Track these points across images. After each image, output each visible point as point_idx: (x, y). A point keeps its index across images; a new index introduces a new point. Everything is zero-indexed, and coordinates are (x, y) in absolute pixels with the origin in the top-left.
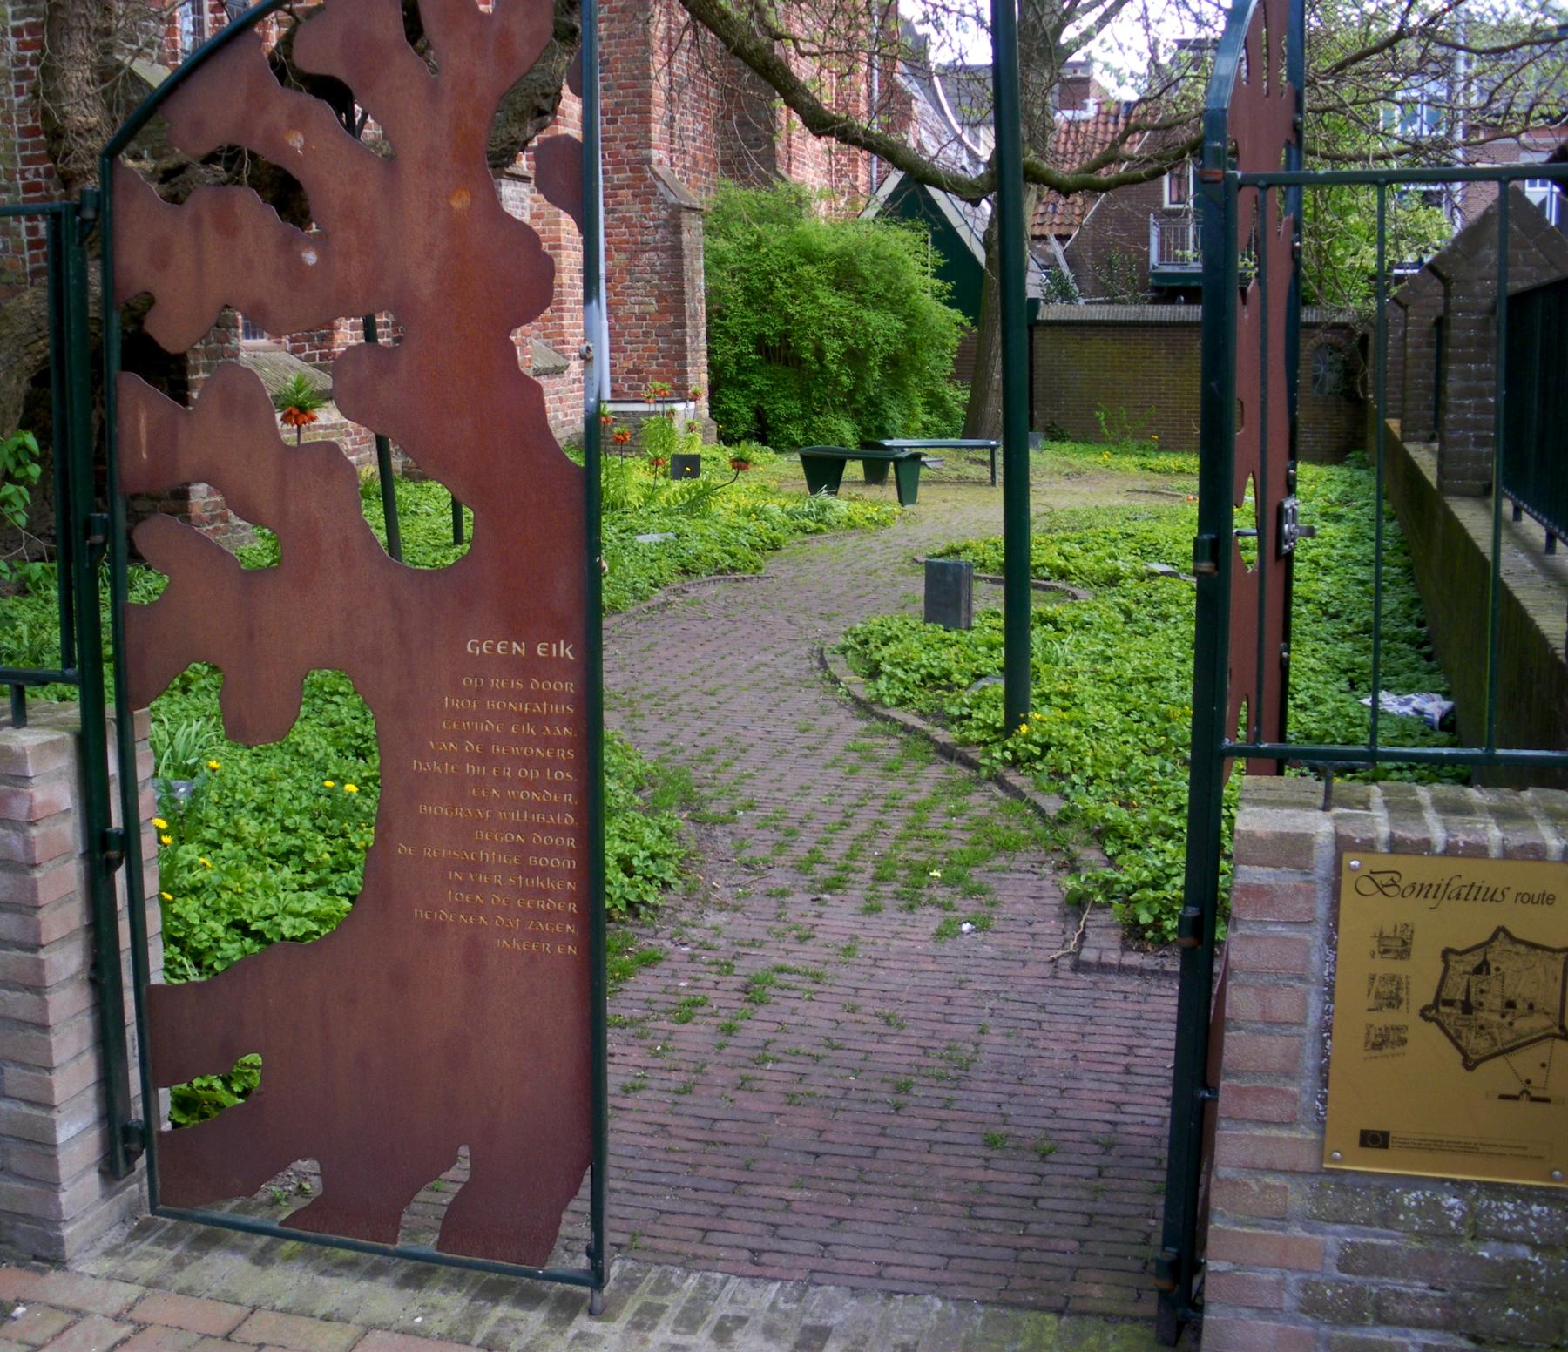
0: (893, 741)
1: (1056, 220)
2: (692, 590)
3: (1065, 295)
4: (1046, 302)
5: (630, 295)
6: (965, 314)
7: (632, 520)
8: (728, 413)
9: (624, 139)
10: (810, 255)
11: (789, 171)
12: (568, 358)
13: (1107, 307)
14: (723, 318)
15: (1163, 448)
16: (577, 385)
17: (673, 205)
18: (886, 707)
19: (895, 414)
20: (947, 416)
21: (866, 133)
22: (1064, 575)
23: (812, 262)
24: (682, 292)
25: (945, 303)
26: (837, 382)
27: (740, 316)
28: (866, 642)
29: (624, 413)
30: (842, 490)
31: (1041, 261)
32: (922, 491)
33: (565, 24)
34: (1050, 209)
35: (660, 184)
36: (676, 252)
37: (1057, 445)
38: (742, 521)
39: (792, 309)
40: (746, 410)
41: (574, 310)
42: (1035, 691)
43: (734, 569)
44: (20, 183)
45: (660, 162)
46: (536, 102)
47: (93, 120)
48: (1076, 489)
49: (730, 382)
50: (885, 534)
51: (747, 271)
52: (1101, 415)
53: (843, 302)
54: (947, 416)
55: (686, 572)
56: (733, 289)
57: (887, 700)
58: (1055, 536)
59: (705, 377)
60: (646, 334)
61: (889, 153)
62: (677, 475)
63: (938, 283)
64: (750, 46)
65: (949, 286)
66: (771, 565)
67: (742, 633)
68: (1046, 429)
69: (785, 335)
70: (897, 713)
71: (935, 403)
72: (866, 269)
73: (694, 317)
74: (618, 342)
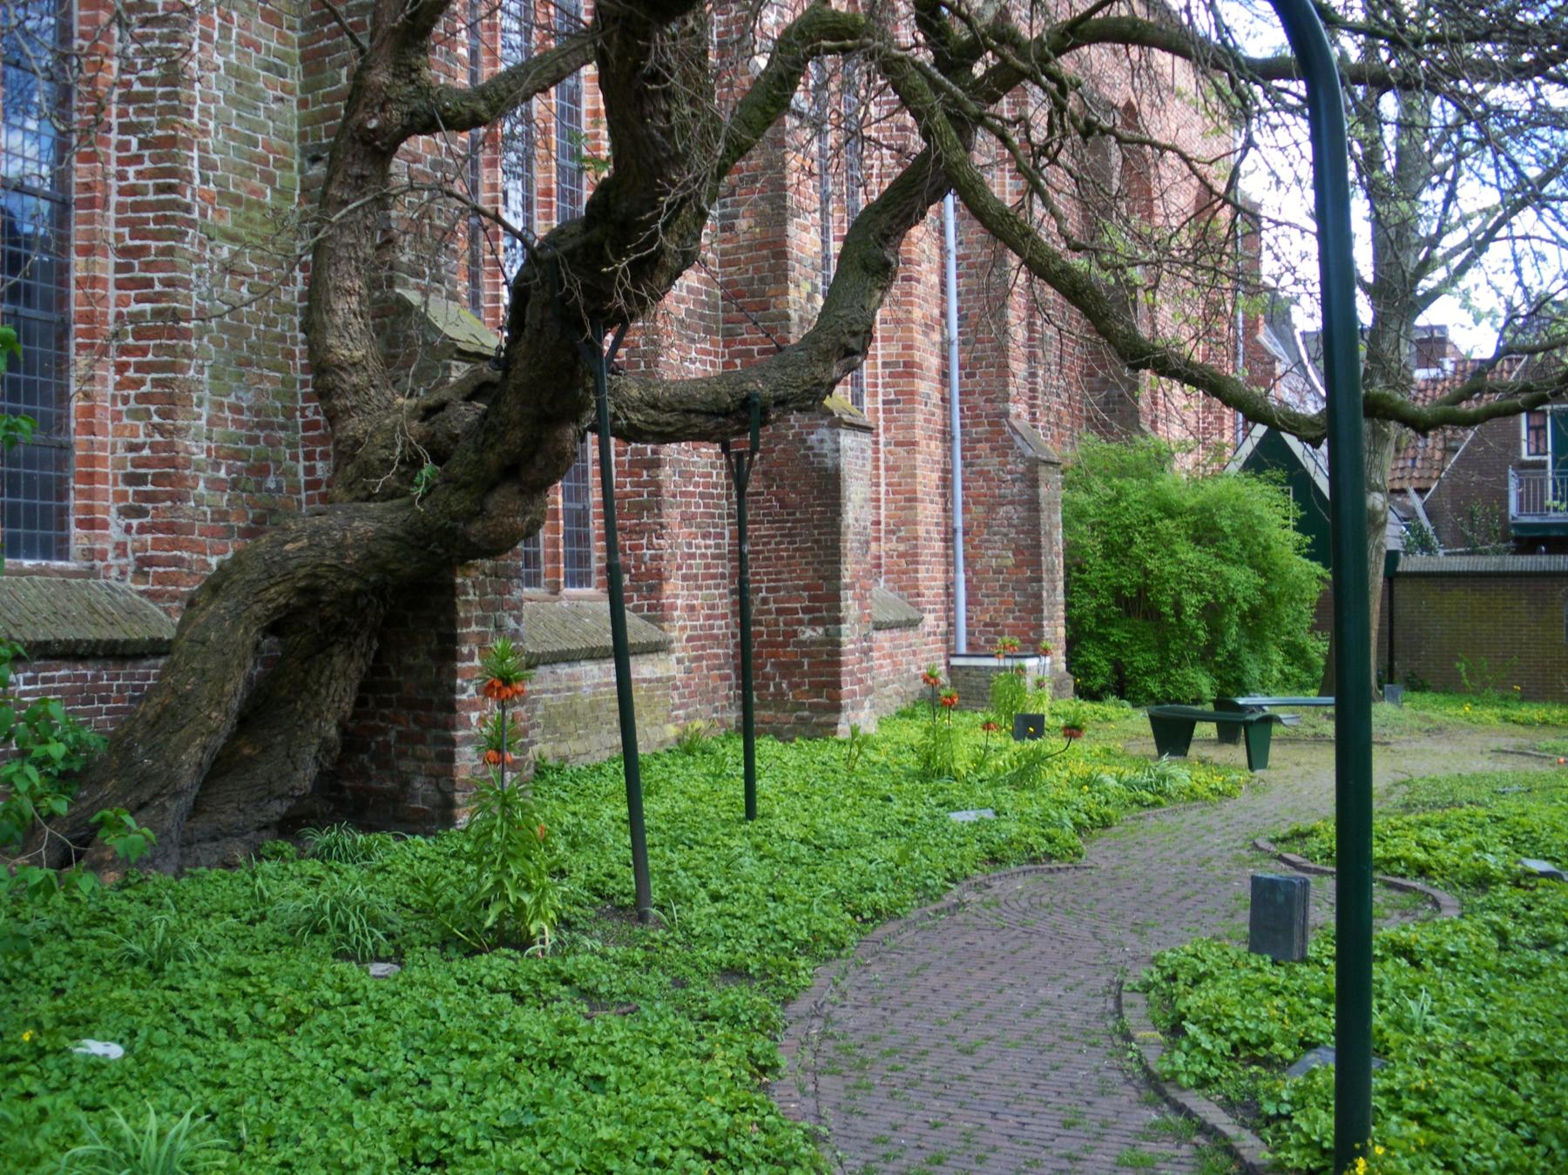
0: (1186, 1150)
1: (1416, 474)
2: (997, 883)
3: (1425, 546)
4: (1406, 553)
5: (987, 549)
6: (1325, 566)
7: (955, 790)
8: (1087, 666)
9: (983, 393)
10: (1169, 511)
11: (1155, 429)
12: (923, 611)
13: (1466, 559)
14: (1082, 571)
15: (1527, 697)
16: (932, 638)
17: (1030, 459)
18: (1181, 1088)
19: (1253, 670)
20: (1308, 667)
21: (1188, 363)
22: (1422, 871)
23: (1171, 517)
24: (1038, 546)
25: (1305, 556)
26: (1194, 637)
27: (1098, 568)
28: (1174, 978)
29: (976, 668)
30: (1193, 751)
31: (1401, 514)
32: (1275, 751)
33: (877, 258)
34: (1409, 463)
35: (1017, 438)
36: (1033, 505)
37: (1417, 696)
38: (1071, 794)
39: (1151, 564)
40: (1103, 663)
41: (930, 563)
42: (1378, 1083)
43: (1049, 857)
44: (300, 420)
45: (1018, 416)
46: (843, 340)
47: (358, 354)
48: (1436, 748)
49: (1091, 635)
50: (1228, 807)
51: (1107, 525)
52: (1461, 666)
53: (1203, 556)
54: (1308, 667)
55: (994, 860)
56: (1093, 545)
57: (1184, 1079)
58: (1412, 818)
59: (1062, 632)
60: (1002, 587)
61: (1253, 412)
62: (1019, 735)
63: (1298, 536)
64: (1055, 267)
65: (1308, 540)
66: (1096, 851)
67: (1034, 950)
68: (1407, 680)
69: (1142, 590)
70: (1195, 1101)
71: (1295, 653)
72: (1225, 524)
73: (1051, 571)
74: (975, 595)
